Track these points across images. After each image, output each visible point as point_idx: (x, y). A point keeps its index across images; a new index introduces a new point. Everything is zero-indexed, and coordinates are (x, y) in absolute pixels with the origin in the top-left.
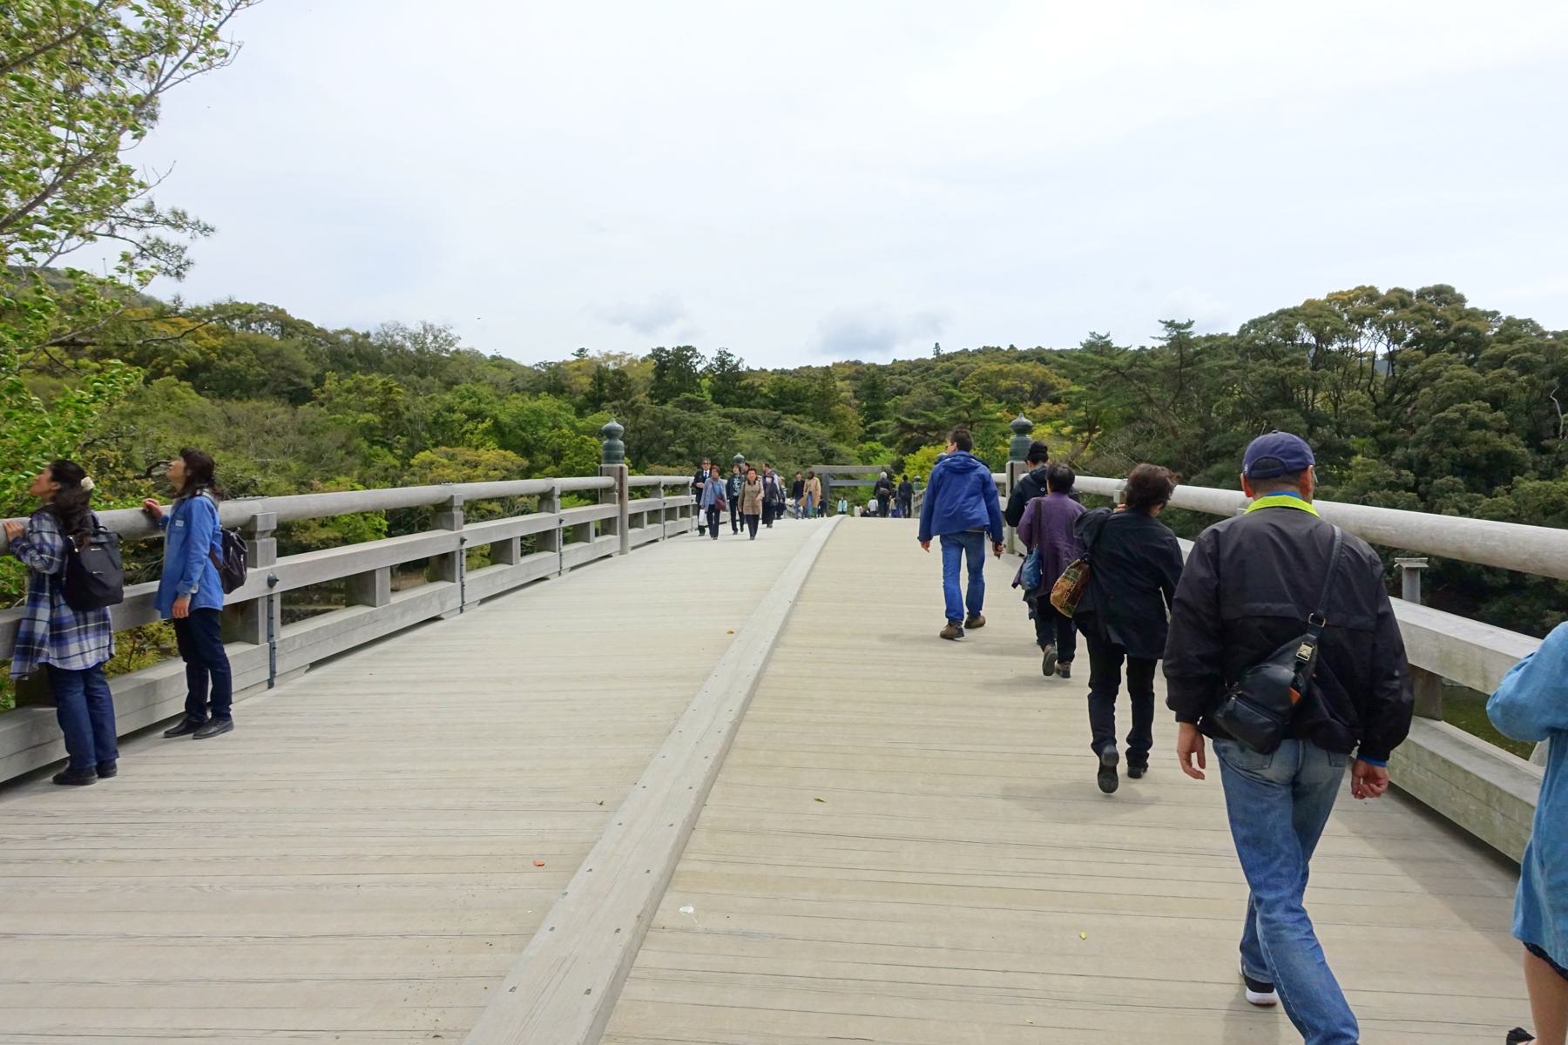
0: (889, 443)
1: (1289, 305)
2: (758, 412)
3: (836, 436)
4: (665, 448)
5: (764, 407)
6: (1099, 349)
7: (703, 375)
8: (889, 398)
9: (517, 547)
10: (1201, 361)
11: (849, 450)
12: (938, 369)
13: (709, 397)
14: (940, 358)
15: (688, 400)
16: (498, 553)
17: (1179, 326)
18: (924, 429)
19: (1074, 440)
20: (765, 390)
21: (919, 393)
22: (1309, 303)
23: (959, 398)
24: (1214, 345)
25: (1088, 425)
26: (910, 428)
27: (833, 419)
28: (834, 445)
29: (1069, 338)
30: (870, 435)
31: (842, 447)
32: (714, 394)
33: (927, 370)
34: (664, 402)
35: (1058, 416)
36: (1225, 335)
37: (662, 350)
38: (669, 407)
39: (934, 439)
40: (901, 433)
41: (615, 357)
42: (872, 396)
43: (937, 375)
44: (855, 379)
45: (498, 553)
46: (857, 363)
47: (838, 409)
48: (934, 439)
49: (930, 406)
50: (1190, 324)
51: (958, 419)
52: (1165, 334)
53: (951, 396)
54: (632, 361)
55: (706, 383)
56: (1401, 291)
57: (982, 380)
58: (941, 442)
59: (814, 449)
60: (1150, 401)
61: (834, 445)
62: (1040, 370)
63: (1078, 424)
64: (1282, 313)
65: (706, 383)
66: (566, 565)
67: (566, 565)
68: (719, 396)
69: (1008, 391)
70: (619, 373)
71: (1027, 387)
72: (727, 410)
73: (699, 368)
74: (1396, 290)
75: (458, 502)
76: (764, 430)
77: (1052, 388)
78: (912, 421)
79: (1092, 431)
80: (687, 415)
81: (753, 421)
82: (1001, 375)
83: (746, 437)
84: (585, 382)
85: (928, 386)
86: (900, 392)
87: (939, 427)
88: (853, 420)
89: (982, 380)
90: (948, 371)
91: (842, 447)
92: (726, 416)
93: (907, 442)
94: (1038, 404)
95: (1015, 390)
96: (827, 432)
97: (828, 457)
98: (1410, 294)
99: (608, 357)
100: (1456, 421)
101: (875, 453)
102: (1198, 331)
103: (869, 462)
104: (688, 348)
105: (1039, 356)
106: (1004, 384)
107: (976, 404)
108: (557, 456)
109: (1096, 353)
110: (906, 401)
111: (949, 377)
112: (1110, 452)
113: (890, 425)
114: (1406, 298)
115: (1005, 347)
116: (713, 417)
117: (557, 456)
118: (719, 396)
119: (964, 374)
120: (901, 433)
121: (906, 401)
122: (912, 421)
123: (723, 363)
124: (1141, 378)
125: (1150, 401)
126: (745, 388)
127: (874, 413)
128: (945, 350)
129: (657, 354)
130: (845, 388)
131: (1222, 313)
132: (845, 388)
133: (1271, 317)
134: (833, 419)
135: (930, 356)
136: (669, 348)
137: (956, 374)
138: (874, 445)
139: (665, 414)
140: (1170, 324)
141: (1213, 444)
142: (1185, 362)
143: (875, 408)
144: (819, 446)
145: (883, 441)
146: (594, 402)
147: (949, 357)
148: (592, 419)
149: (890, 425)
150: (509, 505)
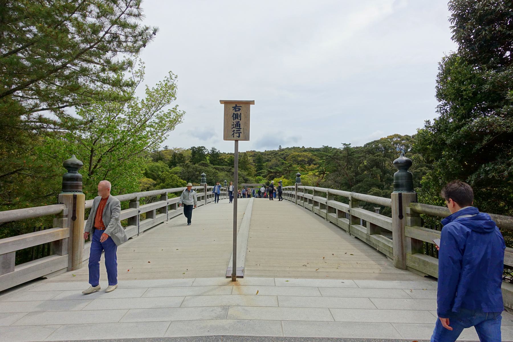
0: (264, 177)
1: (376, 139)
2: (224, 167)
3: (249, 174)
4: (197, 178)
5: (226, 165)
6: (326, 149)
7: (207, 155)
8: (264, 163)
9: (155, 212)
10: (354, 155)
11: (252, 179)
12: (279, 154)
13: (209, 162)
14: (281, 150)
15: (203, 163)
16: (149, 215)
17: (347, 145)
18: (276, 173)
19: (319, 176)
20: (226, 160)
21: (274, 161)
22: (382, 139)
23: (286, 163)
24: (358, 150)
25: (322, 172)
26: (271, 172)
27: (247, 169)
28: (248, 177)
29: (318, 145)
30: (259, 174)
31: (250, 178)
32: (210, 161)
33: (276, 154)
34: (194, 164)
35: (316, 169)
36: (361, 147)
37: (194, 147)
38: (197, 165)
39: (278, 176)
40: (268, 174)
41: (178, 149)
42: (259, 162)
43: (279, 156)
44: (253, 156)
45: (149, 215)
46: (254, 151)
47: (248, 166)
48: (278, 176)
49: (277, 165)
50: (350, 144)
51: (286, 170)
52: (343, 147)
53: (283, 163)
54: (185, 150)
55: (208, 158)
56: (408, 136)
57: (293, 157)
58: (280, 177)
59: (242, 178)
60: (340, 166)
61: (248, 177)
62: (310, 155)
63: (320, 172)
64: (375, 141)
65: (208, 158)
66: (169, 218)
67: (169, 218)
68: (212, 162)
69: (301, 161)
70: (181, 155)
71: (306, 160)
72: (215, 166)
73: (206, 153)
74: (406, 135)
75: (138, 199)
76: (226, 173)
77: (314, 160)
78: (271, 170)
79: (324, 174)
80: (203, 168)
81: (223, 170)
82: (299, 156)
83: (221, 175)
84: (169, 157)
85: (276, 159)
86: (268, 161)
87: (280, 172)
88: (253, 169)
89: (293, 157)
90: (283, 155)
91: (250, 178)
92: (214, 168)
93: (270, 177)
94: (310, 165)
95: (303, 161)
96: (245, 173)
97: (246, 181)
98: (410, 137)
99: (175, 149)
100: (419, 172)
101: (260, 180)
102: (352, 146)
103: (258, 183)
104: (202, 147)
105: (311, 150)
106: (300, 159)
107: (291, 166)
108: (163, 181)
109: (324, 151)
110: (270, 164)
111: (283, 157)
112: (329, 180)
113: (265, 171)
114: (409, 138)
115: (301, 147)
116: (211, 168)
117: (163, 181)
118: (212, 162)
119: (287, 155)
120: (268, 174)
121: (270, 164)
122: (271, 170)
123: (213, 151)
124: (337, 159)
125: (340, 166)
126: (220, 159)
127: (260, 168)
128: (283, 147)
129: (193, 148)
130: (250, 159)
131: (359, 141)
132: (250, 159)
133: (372, 143)
134: (247, 169)
135: (277, 149)
136: (196, 147)
137: (284, 155)
138: (260, 177)
139: (196, 167)
140: (345, 144)
141: (358, 177)
142: (349, 155)
143: (260, 166)
144: (243, 178)
145: (263, 176)
146: (173, 164)
147: (283, 150)
148: (174, 169)
149: (265, 171)
150: (153, 199)
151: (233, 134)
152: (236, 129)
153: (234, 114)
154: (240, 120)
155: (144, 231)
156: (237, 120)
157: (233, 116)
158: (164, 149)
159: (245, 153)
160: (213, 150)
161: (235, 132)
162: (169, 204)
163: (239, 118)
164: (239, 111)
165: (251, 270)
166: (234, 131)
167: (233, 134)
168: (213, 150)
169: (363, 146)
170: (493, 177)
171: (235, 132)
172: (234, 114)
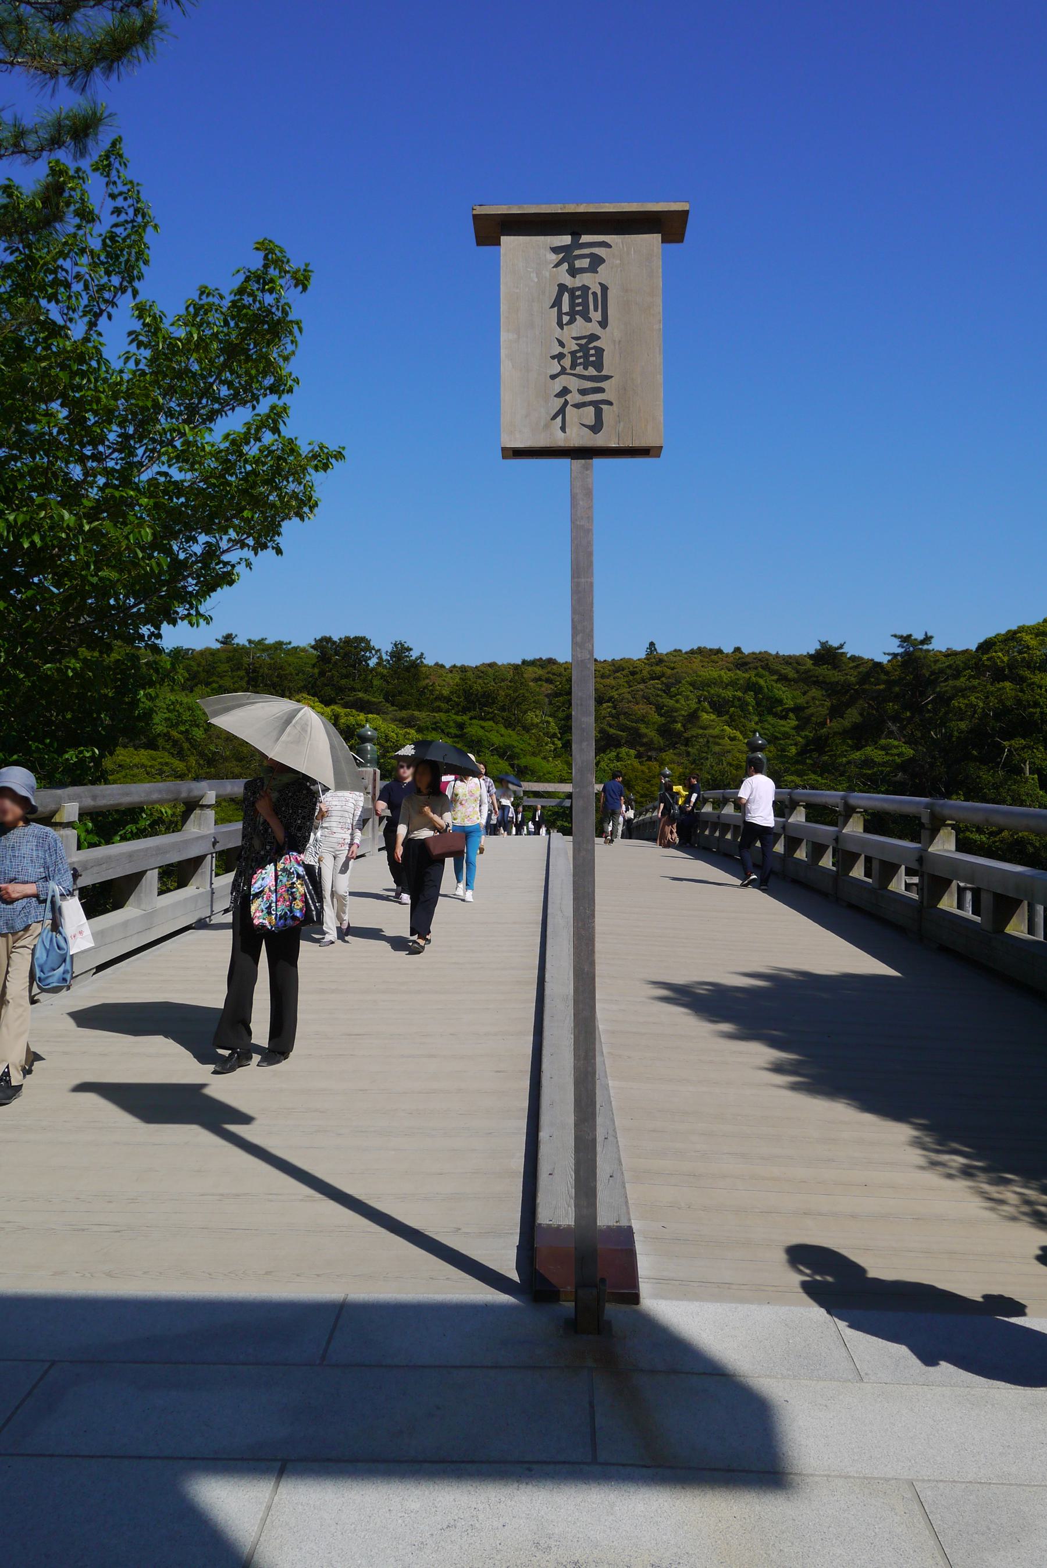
6: (828, 656)
37: (328, 640)
115: (728, 649)
136: (336, 638)
151: (562, 411)
152: (573, 384)
153: (562, 288)
154: (604, 324)
155: (100, 968)
156: (580, 328)
157: (557, 303)
158: (218, 646)
159: (516, 667)
160: (400, 651)
161: (574, 397)
162: (219, 847)
163: (596, 316)
164: (593, 268)
165: (375, 780)
166: (565, 391)
167: (562, 411)
168: (400, 651)
169: (973, 647)
170: (678, 793)
171: (574, 397)
172: (562, 288)
